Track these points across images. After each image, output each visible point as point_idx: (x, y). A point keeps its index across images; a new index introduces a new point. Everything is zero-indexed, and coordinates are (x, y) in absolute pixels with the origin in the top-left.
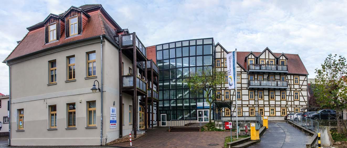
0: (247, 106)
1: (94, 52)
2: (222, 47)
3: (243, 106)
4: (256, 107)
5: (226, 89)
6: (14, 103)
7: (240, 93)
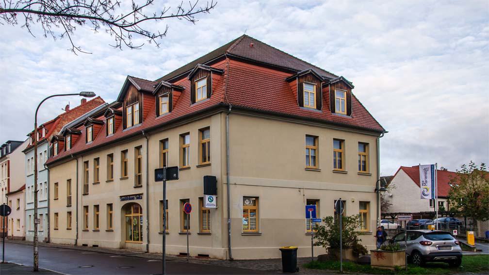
1: (188, 133)
6: (235, 184)
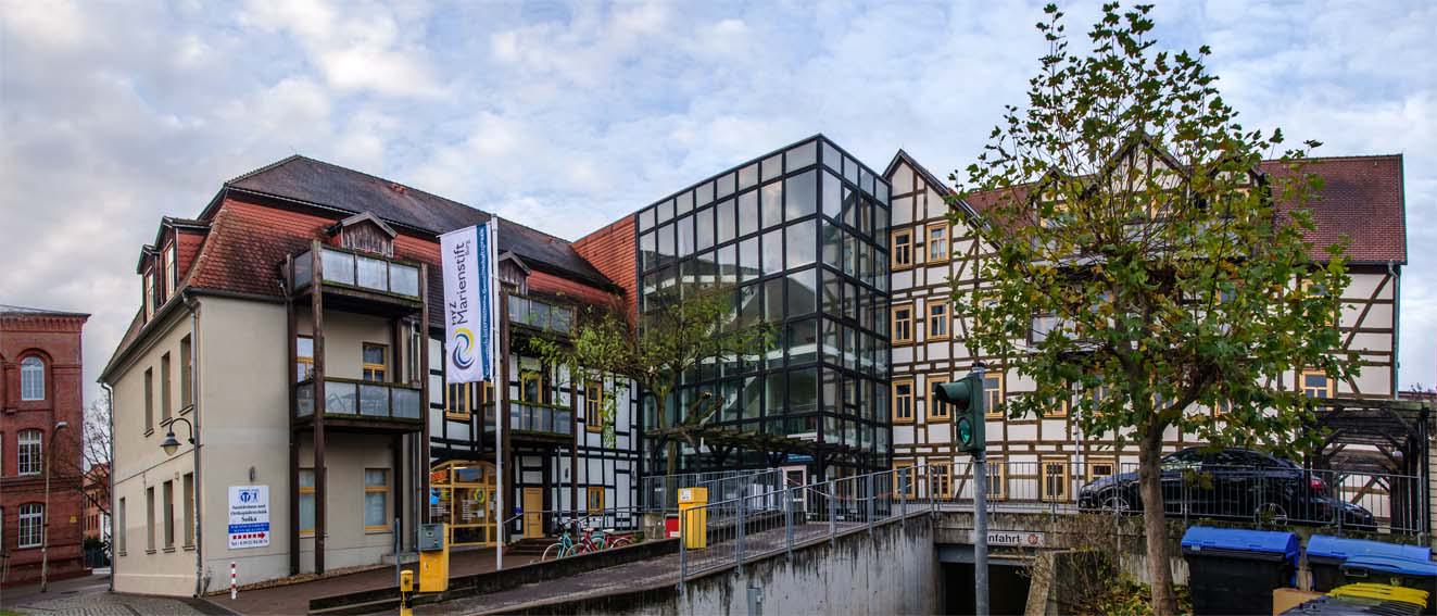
0: (1032, 451)
2: (918, 172)
3: (1011, 448)
4: (1074, 453)
5: (933, 370)
7: (909, 393)
